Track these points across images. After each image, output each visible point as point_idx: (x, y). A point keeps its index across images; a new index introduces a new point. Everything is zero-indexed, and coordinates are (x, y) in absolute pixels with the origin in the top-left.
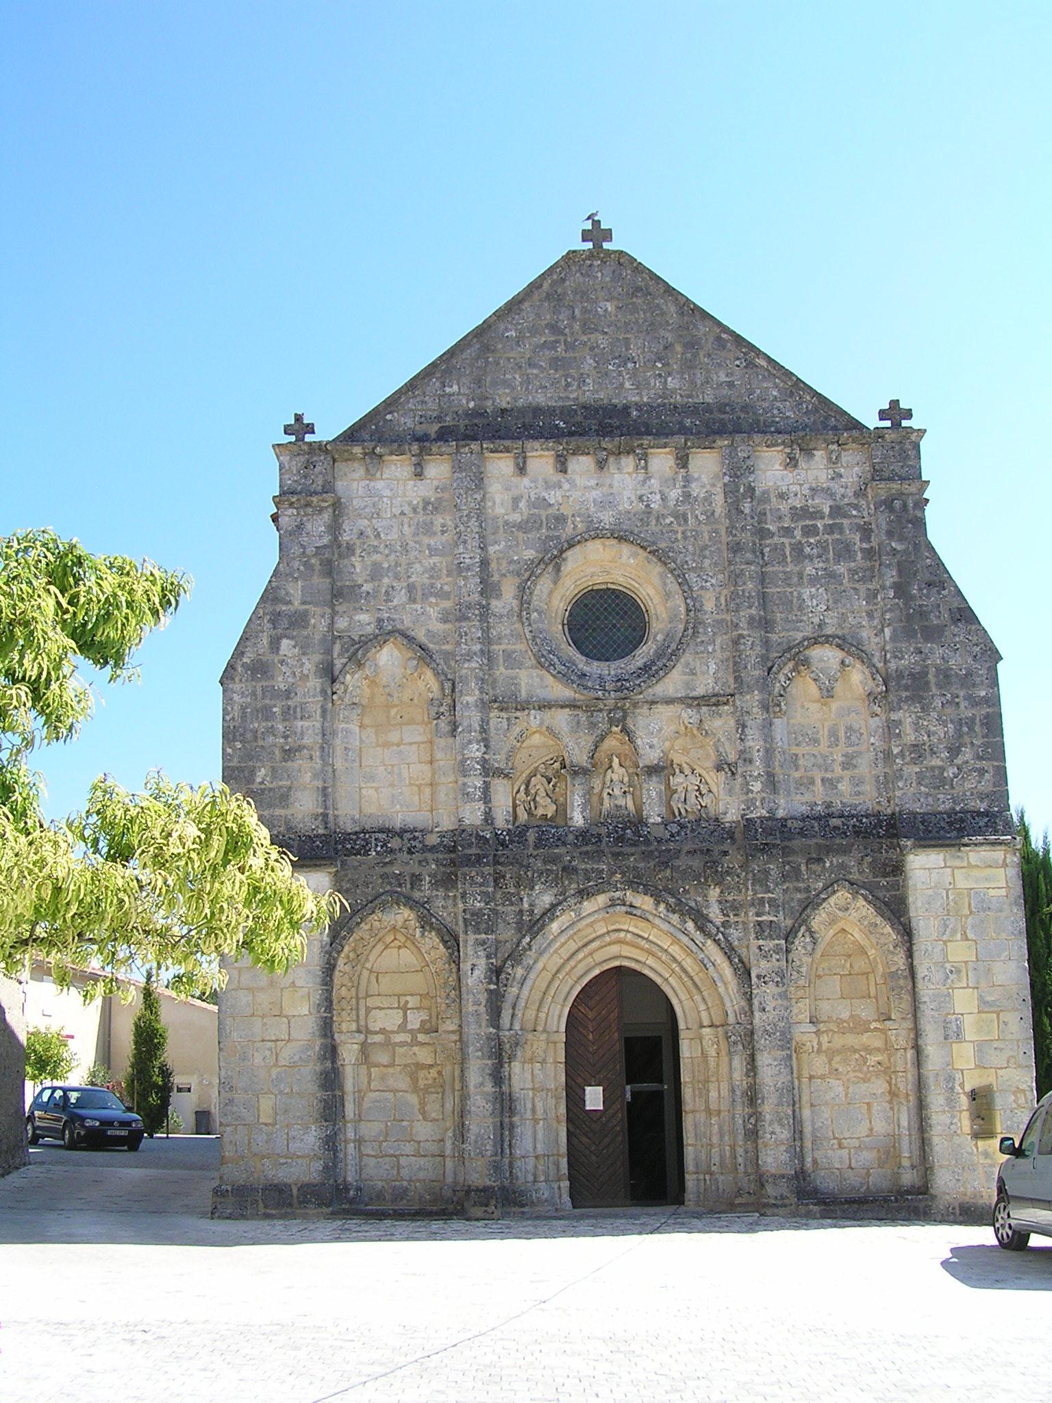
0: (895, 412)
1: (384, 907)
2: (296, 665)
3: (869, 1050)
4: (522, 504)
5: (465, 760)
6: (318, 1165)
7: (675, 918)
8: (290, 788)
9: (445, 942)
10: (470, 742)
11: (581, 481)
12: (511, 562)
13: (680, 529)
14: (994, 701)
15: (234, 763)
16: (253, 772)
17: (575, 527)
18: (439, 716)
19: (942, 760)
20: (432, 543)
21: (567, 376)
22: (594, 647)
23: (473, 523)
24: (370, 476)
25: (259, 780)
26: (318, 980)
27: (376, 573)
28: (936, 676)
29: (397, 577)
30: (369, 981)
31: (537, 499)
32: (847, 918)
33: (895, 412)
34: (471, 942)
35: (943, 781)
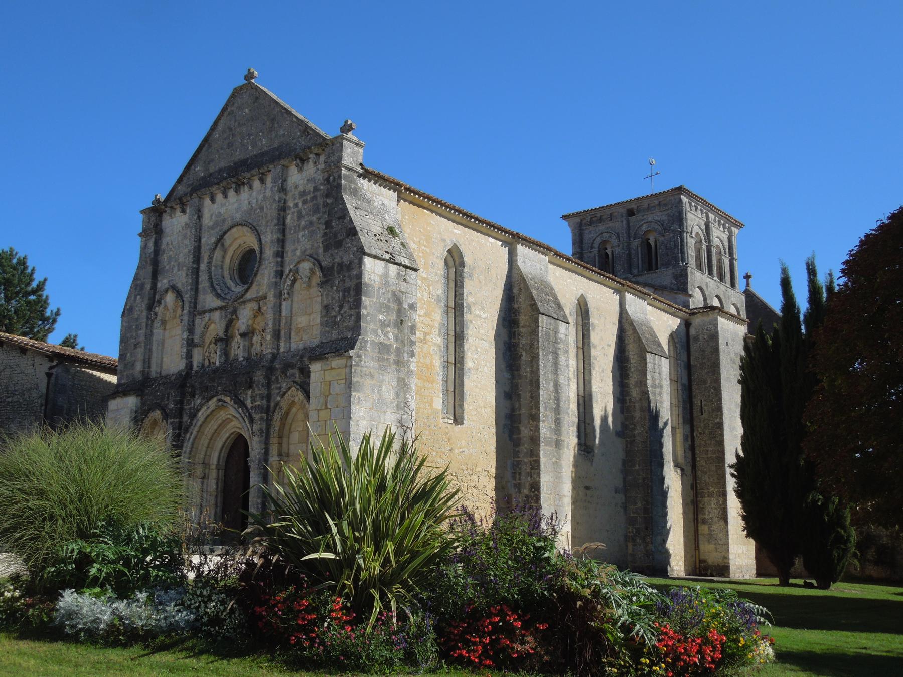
35: (335, 323)
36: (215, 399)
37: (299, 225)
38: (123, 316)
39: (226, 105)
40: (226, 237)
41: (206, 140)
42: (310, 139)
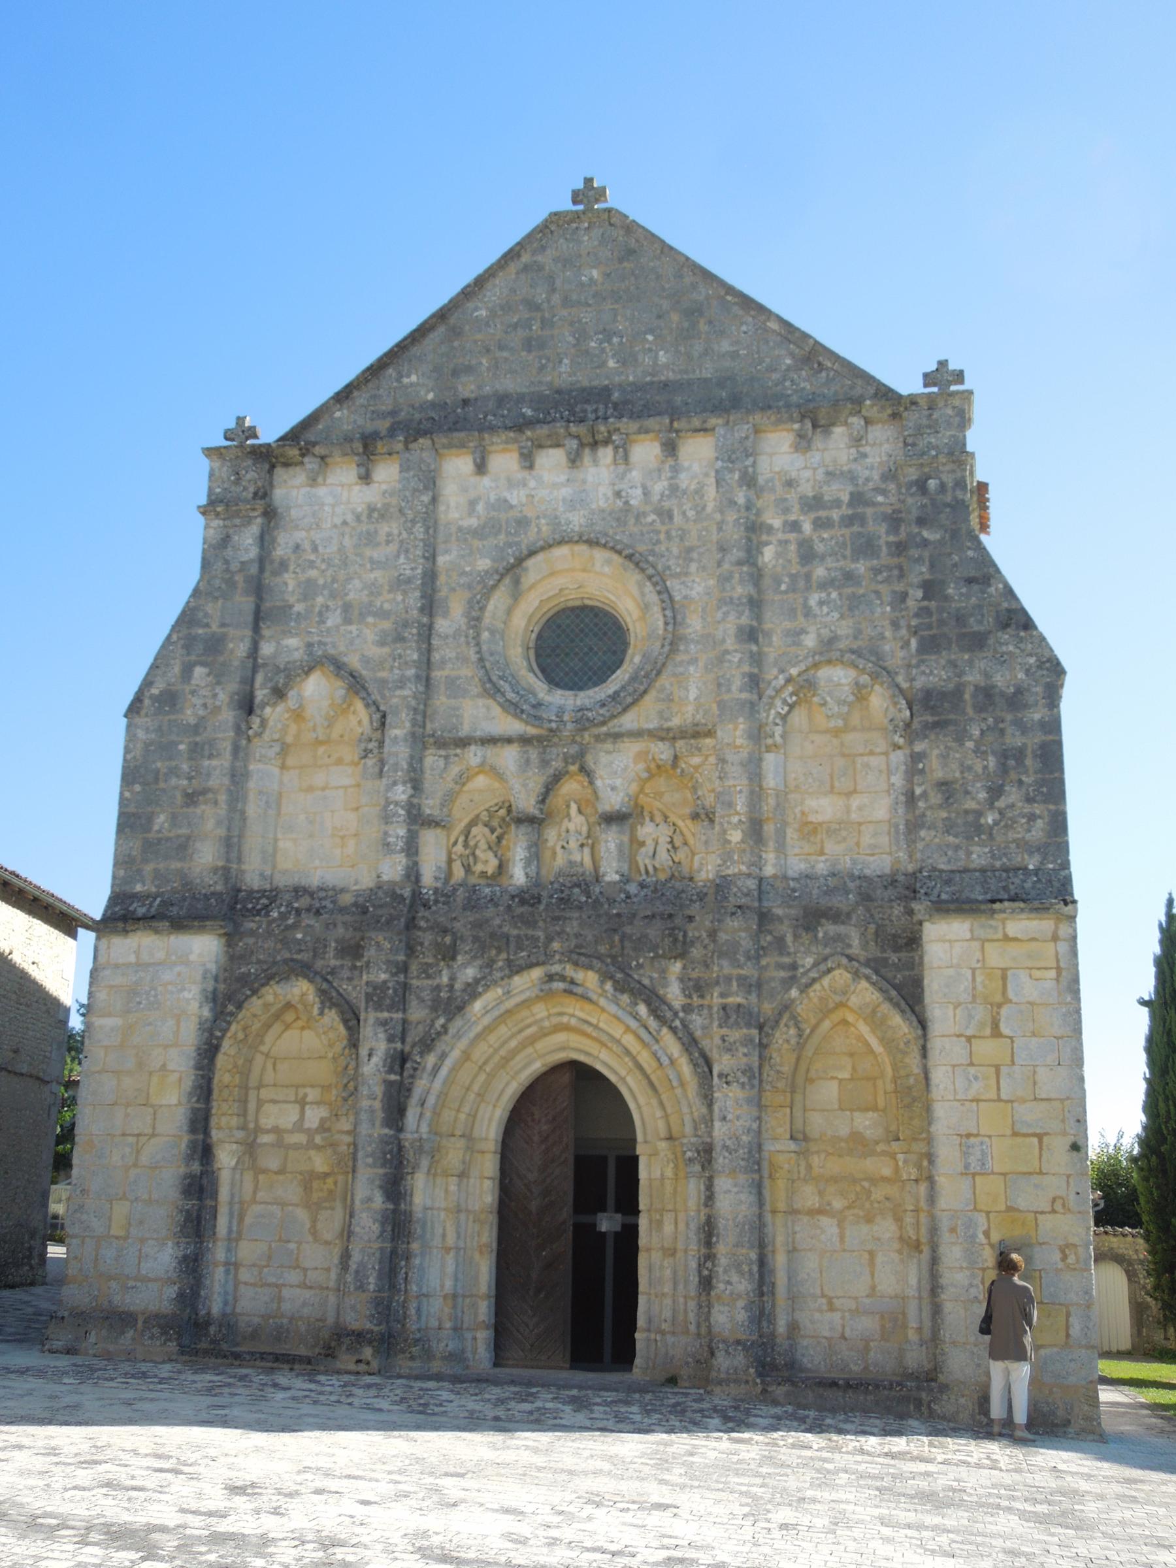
0: (943, 377)
1: (285, 978)
2: (208, 697)
3: (874, 1181)
4: (480, 508)
5: (388, 803)
6: (172, 1291)
7: (625, 998)
8: (188, 838)
9: (345, 1022)
10: (395, 783)
11: (547, 477)
12: (464, 573)
13: (663, 529)
14: (1053, 726)
15: (132, 809)
16: (150, 819)
17: (539, 530)
18: (366, 753)
19: (979, 803)
20: (375, 555)
21: (540, 358)
22: (567, 674)
23: (419, 530)
24: (313, 481)
25: (156, 827)
26: (192, 1063)
27: (309, 590)
28: (974, 696)
29: (333, 596)
30: (264, 1069)
31: (498, 500)
32: (844, 1003)
33: (943, 377)
34: (371, 1021)
35: (978, 829)
36: (537, 973)
37: (808, 577)
38: (134, 709)
39: (521, 245)
40: (530, 563)
41: (441, 315)
42: (829, 381)
